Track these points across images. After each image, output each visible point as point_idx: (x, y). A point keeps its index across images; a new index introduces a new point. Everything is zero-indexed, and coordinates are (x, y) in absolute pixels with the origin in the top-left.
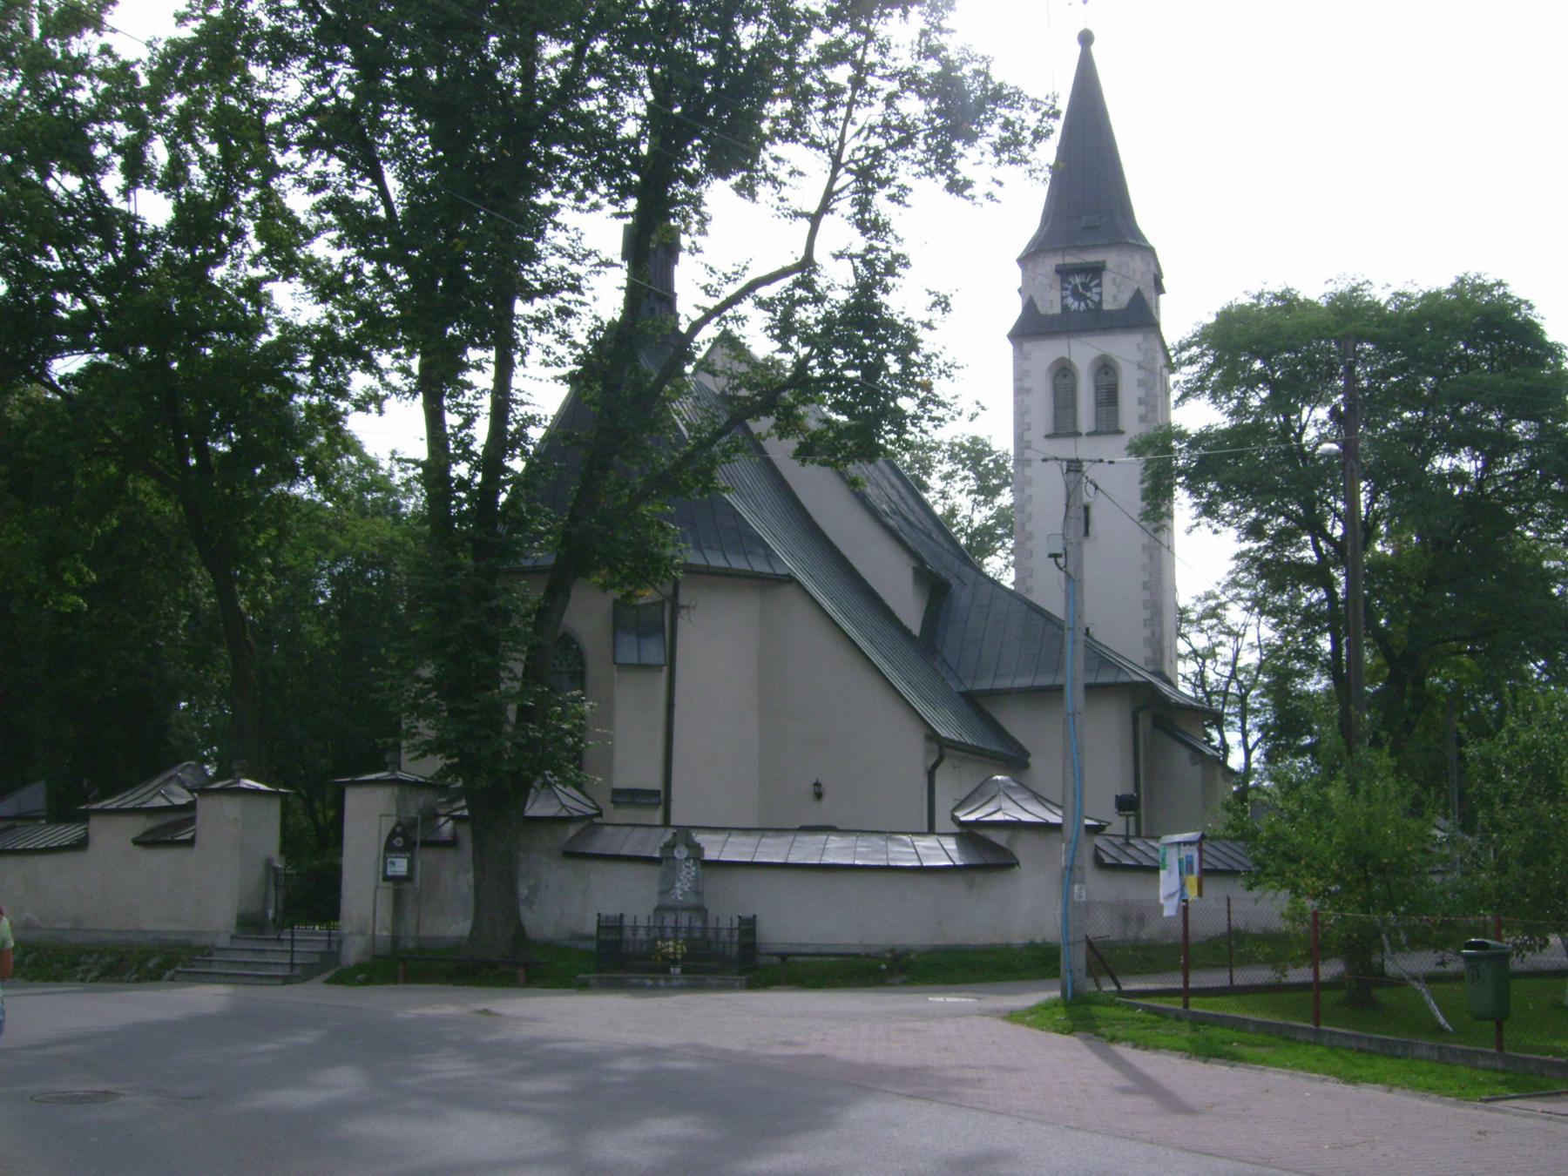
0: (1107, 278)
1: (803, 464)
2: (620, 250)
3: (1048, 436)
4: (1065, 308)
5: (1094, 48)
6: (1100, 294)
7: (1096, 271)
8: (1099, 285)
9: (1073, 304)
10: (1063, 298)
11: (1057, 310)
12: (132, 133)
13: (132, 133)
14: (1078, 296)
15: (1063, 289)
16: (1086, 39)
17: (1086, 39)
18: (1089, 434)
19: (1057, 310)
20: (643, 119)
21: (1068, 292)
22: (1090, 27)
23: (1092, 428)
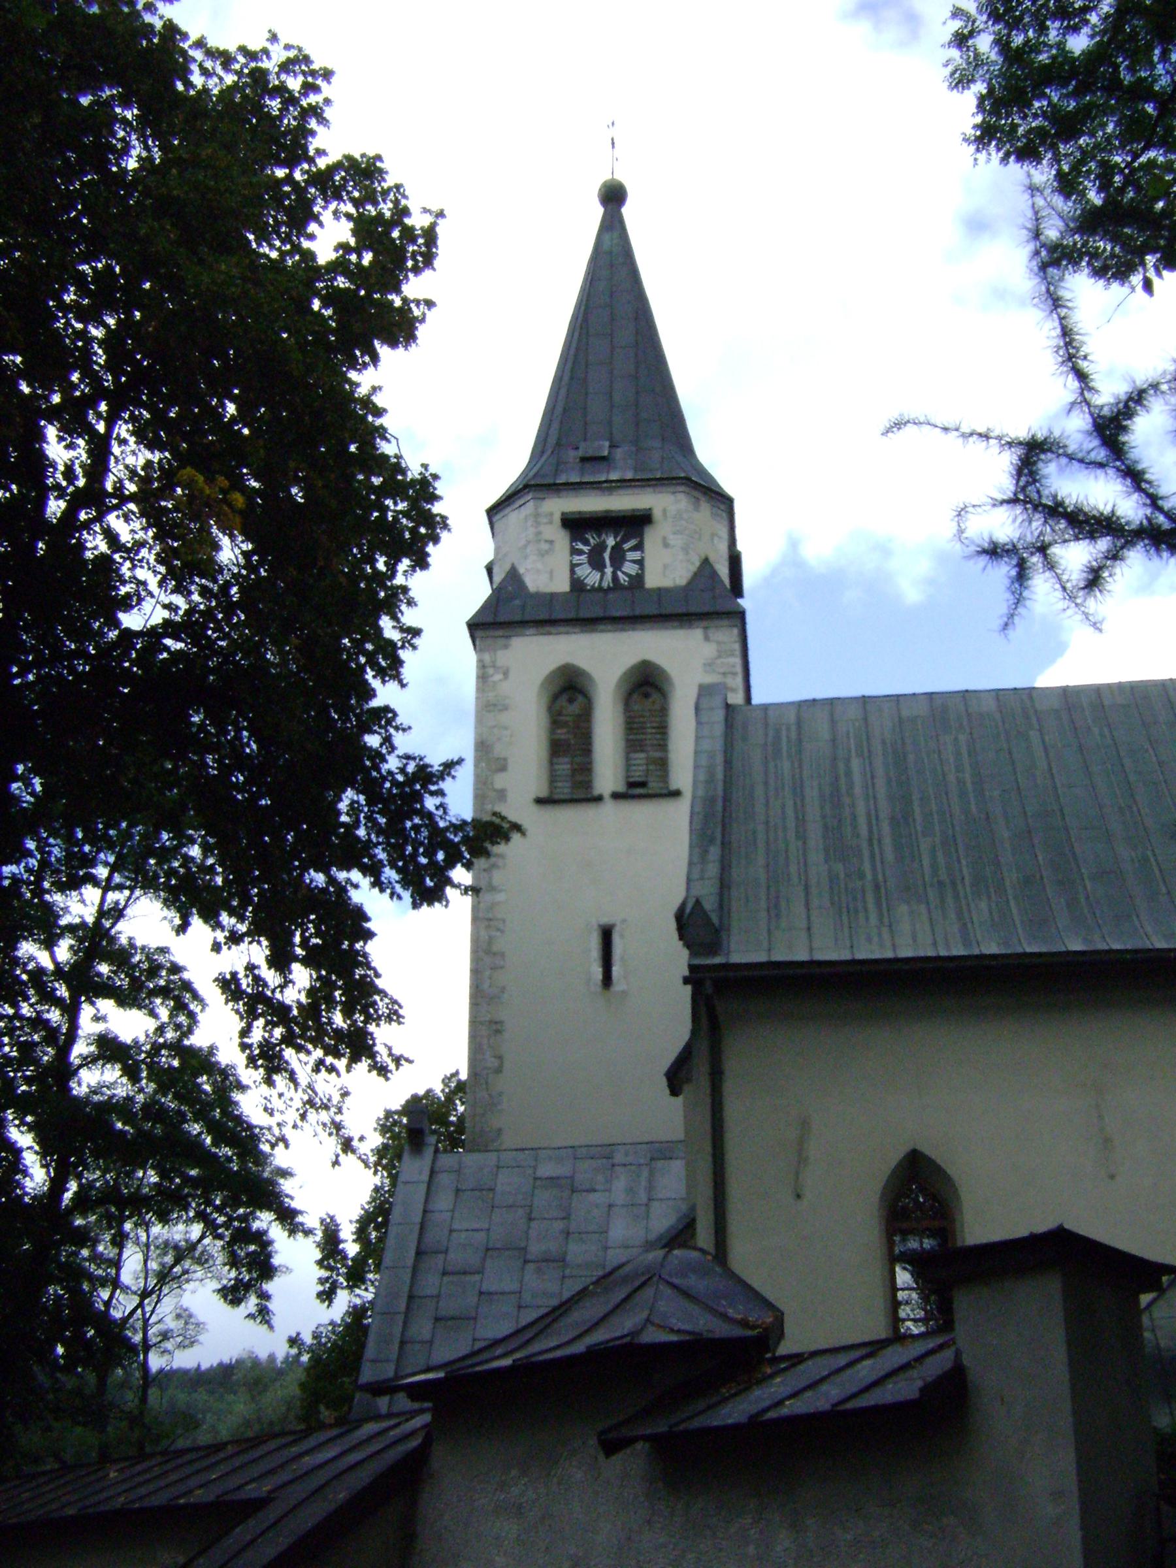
0: (652, 538)
1: (276, 1252)
2: (356, 1213)
3: (540, 801)
4: (577, 585)
5: (628, 211)
6: (640, 563)
7: (638, 523)
8: (639, 547)
9: (592, 578)
10: (573, 567)
11: (562, 585)
12: (441, 1095)
13: (441, 1095)
14: (596, 563)
15: (575, 552)
16: (613, 196)
17: (613, 196)
18: (616, 796)
19: (562, 585)
20: (275, 1220)
21: (584, 558)
22: (620, 177)
23: (621, 788)
